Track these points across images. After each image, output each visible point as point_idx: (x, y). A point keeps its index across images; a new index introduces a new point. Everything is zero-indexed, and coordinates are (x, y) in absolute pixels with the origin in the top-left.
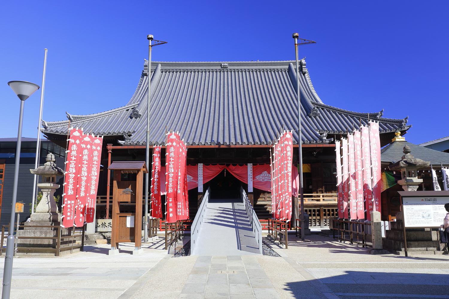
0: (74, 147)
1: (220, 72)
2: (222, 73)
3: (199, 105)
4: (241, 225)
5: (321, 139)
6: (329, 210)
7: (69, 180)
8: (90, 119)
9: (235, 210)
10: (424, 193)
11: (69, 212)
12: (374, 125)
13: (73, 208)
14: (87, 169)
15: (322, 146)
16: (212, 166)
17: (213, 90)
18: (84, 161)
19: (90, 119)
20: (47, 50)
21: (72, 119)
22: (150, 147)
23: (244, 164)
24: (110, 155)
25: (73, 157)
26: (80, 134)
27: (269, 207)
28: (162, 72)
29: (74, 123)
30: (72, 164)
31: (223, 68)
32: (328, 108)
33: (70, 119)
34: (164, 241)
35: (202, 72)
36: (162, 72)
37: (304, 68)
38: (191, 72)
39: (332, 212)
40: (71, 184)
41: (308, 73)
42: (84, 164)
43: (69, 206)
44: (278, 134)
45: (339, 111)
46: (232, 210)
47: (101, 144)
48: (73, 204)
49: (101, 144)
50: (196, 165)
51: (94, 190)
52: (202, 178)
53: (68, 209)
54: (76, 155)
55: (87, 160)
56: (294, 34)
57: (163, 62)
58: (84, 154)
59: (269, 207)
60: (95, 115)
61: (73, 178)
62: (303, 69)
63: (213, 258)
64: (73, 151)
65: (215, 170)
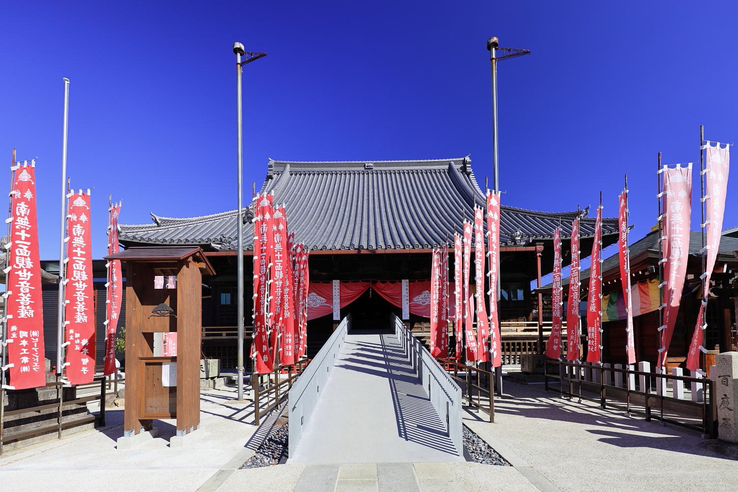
1: (363, 174)
2: (366, 176)
3: (336, 208)
4: (402, 373)
5: (514, 240)
6: (513, 344)
8: (186, 224)
9: (385, 346)
12: (718, 153)
13: (36, 346)
15: (514, 249)
16: (352, 283)
17: (355, 194)
19: (186, 224)
20: (67, 81)
21: (159, 222)
25: (79, 249)
26: (85, 203)
27: (428, 340)
28: (291, 175)
29: (163, 228)
30: (78, 263)
31: (367, 169)
32: (507, 209)
33: (156, 222)
34: (252, 409)
35: (341, 174)
36: (291, 175)
37: (468, 167)
38: (327, 175)
39: (518, 345)
40: (81, 302)
41: (473, 174)
42: (19, 238)
43: (24, 343)
45: (522, 212)
46: (381, 347)
48: (35, 337)
52: (339, 301)
53: (23, 349)
54: (30, 226)
55: (83, 247)
56: (490, 39)
57: (292, 162)
58: (75, 234)
59: (428, 340)
60: (194, 218)
62: (467, 168)
63: (339, 482)
64: (19, 218)
65: (356, 290)
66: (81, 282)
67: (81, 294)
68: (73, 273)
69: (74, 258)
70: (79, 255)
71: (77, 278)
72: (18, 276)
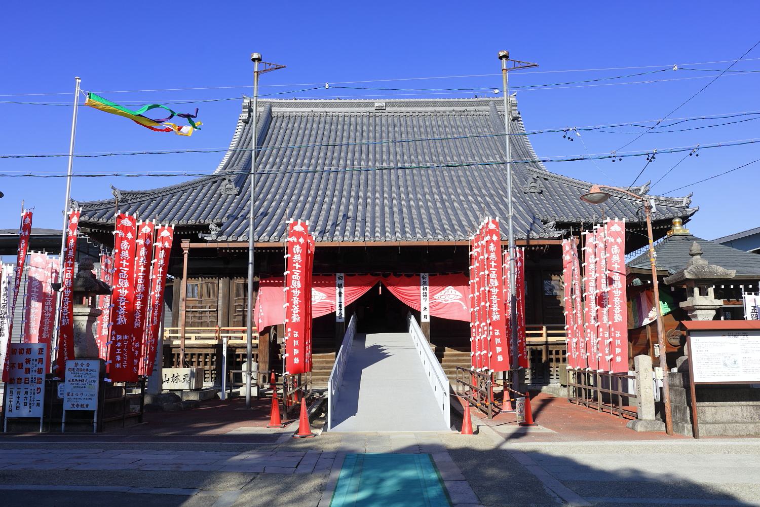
0: (125, 245)
7: (292, 300)
10: (723, 323)
11: (118, 354)
14: (496, 275)
18: (295, 263)
22: (253, 244)
23: (357, 274)
24: (186, 256)
26: (495, 226)
40: (296, 305)
44: (475, 224)
47: (623, 233)
48: (126, 340)
49: (171, 238)
50: (331, 275)
51: (297, 315)
54: (129, 257)
61: (125, 295)
66: (123, 289)
67: (123, 300)
68: (292, 282)
69: (294, 270)
70: (124, 266)
71: (295, 286)
72: (293, 293)
